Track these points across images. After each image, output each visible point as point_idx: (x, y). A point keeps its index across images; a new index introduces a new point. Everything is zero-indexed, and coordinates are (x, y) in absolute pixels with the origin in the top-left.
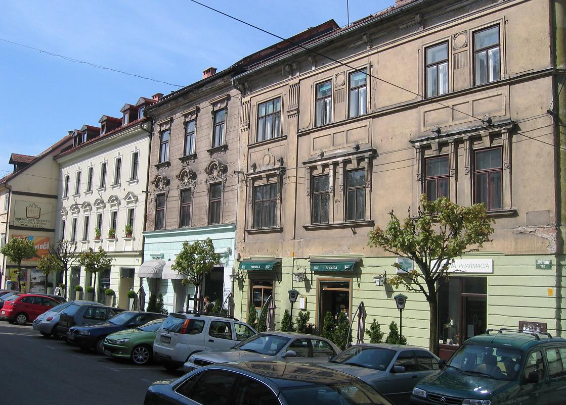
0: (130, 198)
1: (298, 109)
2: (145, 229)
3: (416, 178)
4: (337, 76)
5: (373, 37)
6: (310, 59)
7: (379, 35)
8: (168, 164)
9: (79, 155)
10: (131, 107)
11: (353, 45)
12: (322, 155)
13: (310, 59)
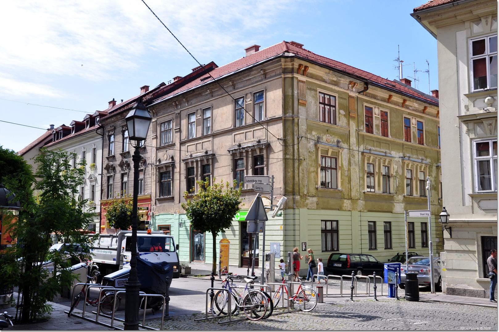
0: (92, 178)
1: (180, 129)
2: (101, 199)
3: (231, 170)
4: (197, 110)
5: (213, 91)
6: (184, 99)
7: (215, 90)
8: (114, 157)
9: (67, 144)
11: (204, 94)
12: (191, 156)
13: (184, 99)
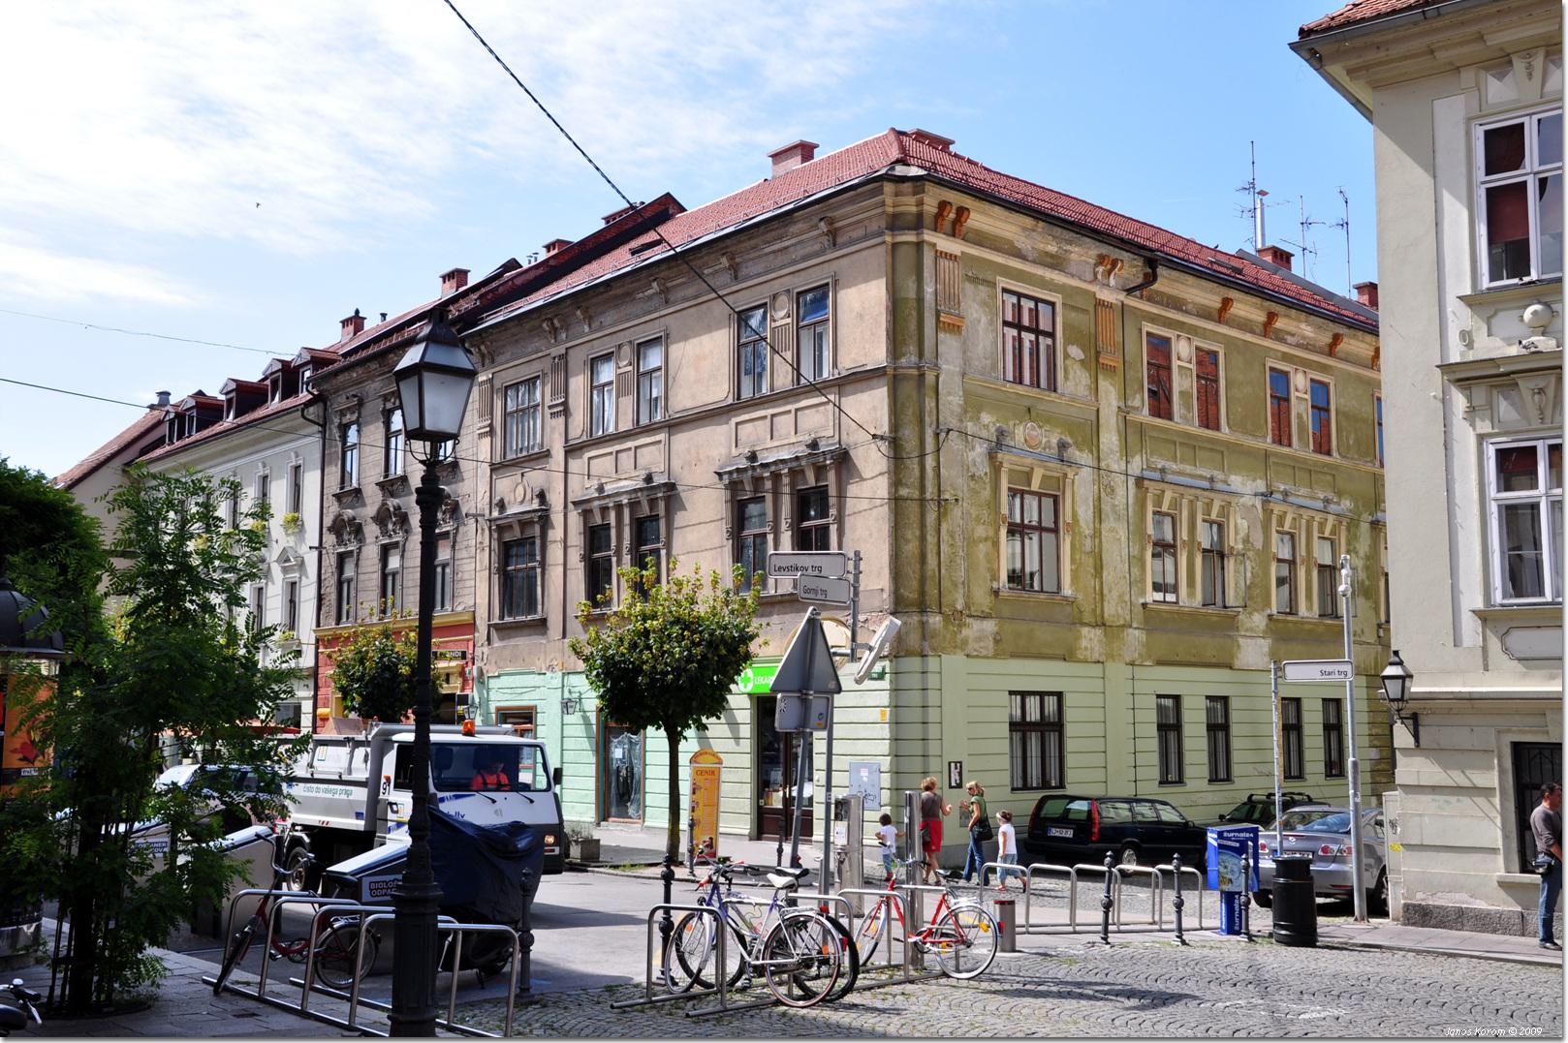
2: (318, 625)
3: (726, 535)
4: (620, 346)
5: (669, 285)
6: (578, 313)
7: (674, 283)
8: (358, 492)
9: (209, 452)
10: (285, 364)
11: (641, 295)
12: (601, 489)
13: (578, 313)
